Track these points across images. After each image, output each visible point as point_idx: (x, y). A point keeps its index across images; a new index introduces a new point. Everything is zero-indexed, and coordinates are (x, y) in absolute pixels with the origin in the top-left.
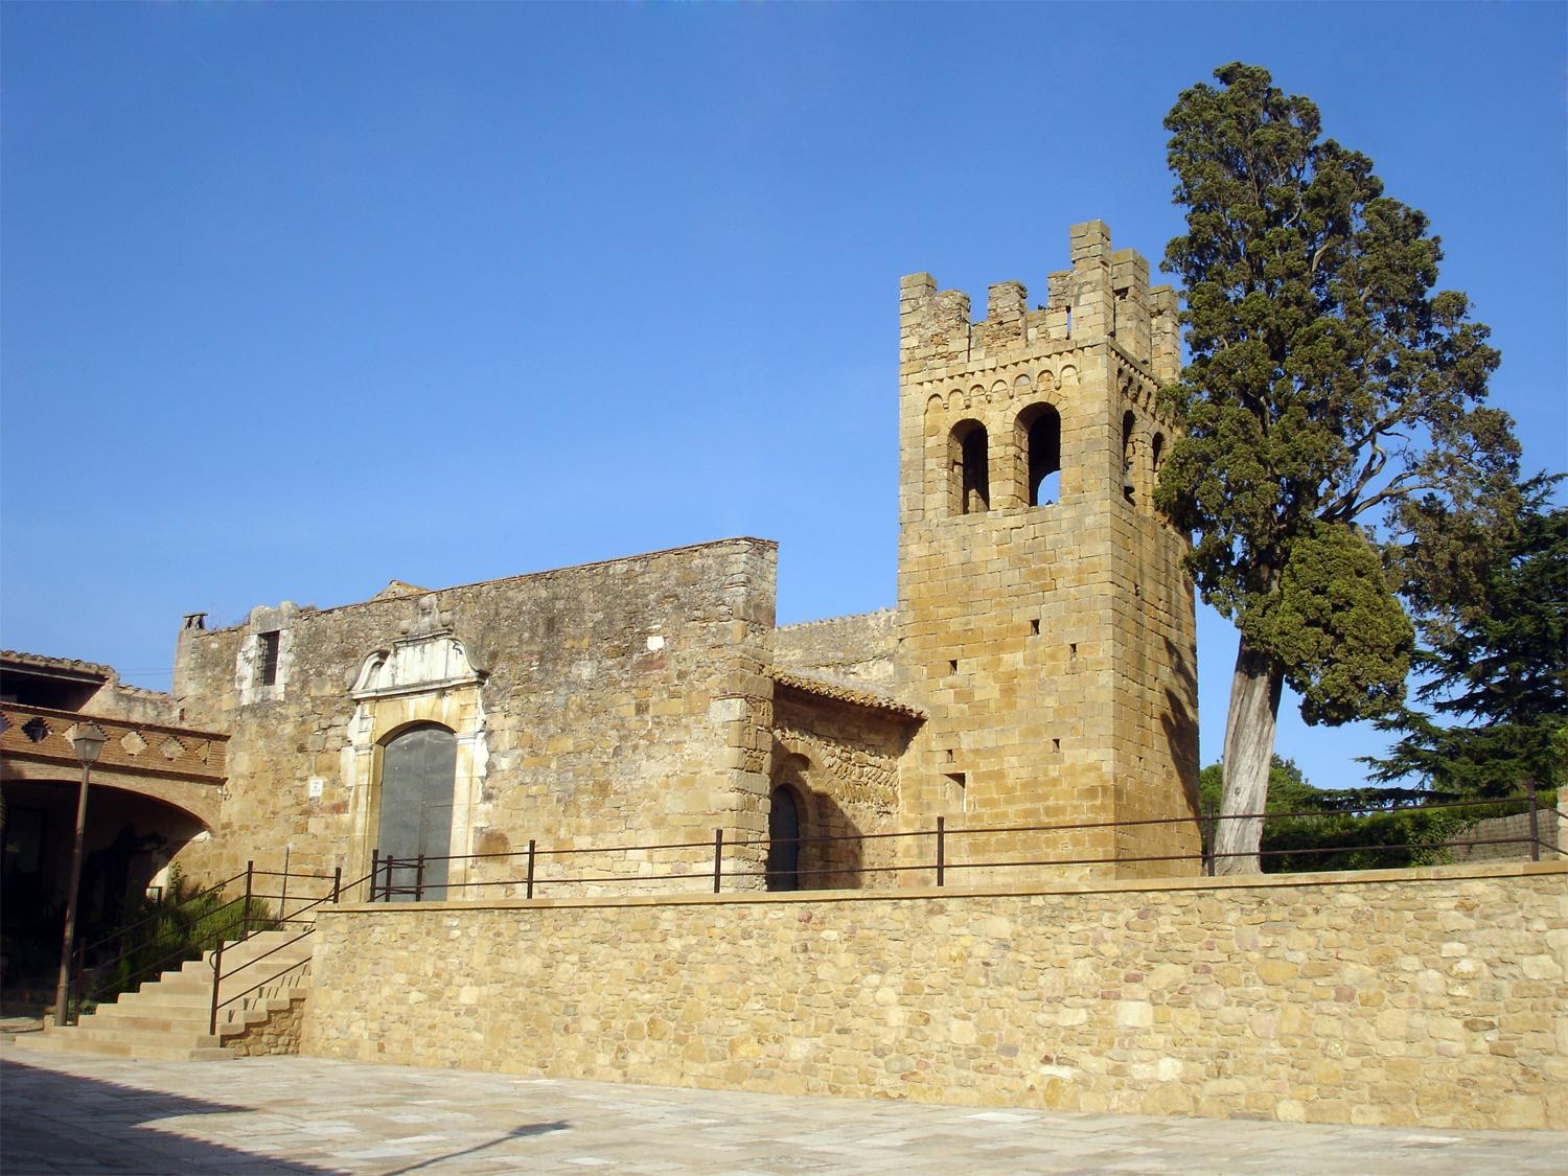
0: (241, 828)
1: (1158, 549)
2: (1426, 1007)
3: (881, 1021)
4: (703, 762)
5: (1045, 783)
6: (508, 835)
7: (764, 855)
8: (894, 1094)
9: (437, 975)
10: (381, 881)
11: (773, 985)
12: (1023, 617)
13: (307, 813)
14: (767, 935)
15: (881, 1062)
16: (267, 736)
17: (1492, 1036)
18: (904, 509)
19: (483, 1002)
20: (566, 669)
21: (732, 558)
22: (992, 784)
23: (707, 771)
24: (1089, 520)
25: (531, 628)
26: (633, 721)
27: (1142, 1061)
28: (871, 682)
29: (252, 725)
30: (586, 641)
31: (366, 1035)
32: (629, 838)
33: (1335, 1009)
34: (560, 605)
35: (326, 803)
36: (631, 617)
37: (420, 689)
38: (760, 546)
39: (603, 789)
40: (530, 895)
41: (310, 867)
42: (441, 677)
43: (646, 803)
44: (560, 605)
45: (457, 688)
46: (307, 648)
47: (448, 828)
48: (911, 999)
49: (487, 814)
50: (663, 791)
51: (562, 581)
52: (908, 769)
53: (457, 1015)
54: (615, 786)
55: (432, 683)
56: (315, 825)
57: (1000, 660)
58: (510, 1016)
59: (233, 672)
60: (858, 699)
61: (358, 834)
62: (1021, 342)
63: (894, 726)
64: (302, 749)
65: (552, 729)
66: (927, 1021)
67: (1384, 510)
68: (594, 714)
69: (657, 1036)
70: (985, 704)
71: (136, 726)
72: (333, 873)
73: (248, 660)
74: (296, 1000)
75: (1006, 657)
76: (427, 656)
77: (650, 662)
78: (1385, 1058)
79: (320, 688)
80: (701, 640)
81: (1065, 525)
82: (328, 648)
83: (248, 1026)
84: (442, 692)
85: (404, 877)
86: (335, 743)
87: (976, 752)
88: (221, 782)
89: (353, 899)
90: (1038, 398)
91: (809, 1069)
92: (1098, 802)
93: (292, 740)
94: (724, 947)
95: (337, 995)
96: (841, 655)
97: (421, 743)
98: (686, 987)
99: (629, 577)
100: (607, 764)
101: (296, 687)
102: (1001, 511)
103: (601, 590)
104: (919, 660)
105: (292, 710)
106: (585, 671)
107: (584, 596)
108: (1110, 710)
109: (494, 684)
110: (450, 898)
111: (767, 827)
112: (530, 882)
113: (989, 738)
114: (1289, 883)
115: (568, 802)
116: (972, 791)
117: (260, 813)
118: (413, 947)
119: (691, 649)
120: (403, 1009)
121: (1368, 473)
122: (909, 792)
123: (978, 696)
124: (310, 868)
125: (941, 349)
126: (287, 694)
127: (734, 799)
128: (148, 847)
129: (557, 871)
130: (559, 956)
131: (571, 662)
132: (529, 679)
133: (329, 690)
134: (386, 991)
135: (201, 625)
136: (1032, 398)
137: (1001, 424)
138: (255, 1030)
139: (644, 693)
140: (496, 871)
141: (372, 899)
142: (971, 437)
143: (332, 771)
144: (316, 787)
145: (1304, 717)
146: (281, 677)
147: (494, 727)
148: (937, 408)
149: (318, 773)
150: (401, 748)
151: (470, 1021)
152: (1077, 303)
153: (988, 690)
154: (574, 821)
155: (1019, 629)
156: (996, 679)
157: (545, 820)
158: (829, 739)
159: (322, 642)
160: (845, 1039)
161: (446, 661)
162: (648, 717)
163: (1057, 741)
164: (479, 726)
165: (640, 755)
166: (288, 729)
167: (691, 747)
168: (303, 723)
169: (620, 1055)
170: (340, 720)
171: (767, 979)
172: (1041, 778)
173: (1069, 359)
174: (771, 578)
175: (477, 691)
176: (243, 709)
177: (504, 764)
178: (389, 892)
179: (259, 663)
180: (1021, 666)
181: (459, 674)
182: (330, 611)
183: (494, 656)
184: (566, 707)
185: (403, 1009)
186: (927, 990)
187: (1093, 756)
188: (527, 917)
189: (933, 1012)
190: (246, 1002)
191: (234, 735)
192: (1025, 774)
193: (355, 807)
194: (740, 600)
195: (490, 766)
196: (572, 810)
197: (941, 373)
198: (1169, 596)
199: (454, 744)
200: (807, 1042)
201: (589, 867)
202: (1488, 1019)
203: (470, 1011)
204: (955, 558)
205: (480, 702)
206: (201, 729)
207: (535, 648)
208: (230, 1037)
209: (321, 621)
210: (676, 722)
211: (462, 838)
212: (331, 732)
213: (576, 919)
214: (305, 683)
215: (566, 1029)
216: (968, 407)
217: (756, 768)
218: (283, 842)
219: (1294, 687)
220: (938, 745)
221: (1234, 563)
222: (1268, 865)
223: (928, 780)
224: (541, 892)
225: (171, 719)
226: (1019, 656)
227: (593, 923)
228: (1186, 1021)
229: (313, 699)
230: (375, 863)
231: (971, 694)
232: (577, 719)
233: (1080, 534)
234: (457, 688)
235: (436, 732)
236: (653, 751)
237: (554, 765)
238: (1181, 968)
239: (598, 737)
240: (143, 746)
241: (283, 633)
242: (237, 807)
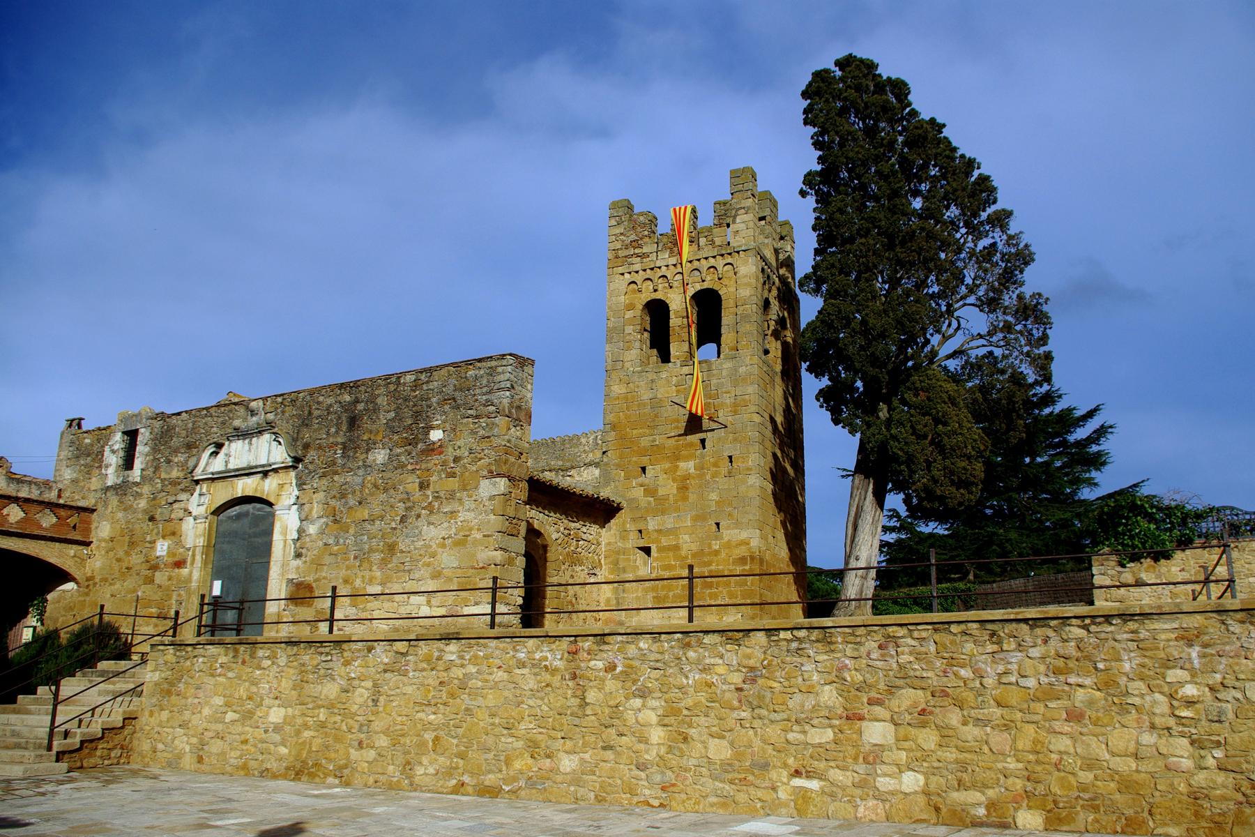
0: (101, 580)
2: (1153, 726)
3: (644, 740)
4: (468, 528)
5: (709, 554)
6: (314, 585)
7: (520, 601)
8: (656, 803)
9: (250, 698)
10: (206, 619)
11: (545, 708)
13: (155, 568)
14: (540, 667)
15: (643, 775)
16: (125, 510)
17: (1219, 753)
18: (609, 360)
19: (287, 720)
20: (364, 456)
21: (500, 369)
22: (671, 554)
24: (742, 370)
25: (337, 425)
27: (885, 775)
28: (583, 480)
29: (114, 500)
31: (187, 748)
32: (410, 586)
33: (1067, 729)
35: (170, 560)
36: (417, 415)
37: (247, 472)
38: (523, 362)
39: (392, 548)
40: (331, 631)
41: (154, 610)
42: (264, 462)
43: (426, 559)
44: (361, 406)
45: (276, 471)
46: (163, 438)
47: (265, 579)
48: (671, 720)
49: (298, 568)
51: (362, 388)
52: (609, 544)
53: (266, 732)
54: (402, 546)
55: (256, 467)
56: (160, 577)
57: (677, 467)
58: (312, 733)
59: (101, 461)
60: (578, 491)
61: (194, 585)
63: (600, 510)
64: (152, 519)
65: (352, 502)
66: (685, 739)
68: (386, 490)
69: (440, 751)
70: (665, 498)
71: (16, 500)
72: (172, 613)
73: (113, 452)
74: (129, 719)
75: (682, 465)
76: (254, 446)
78: (1117, 772)
80: (473, 433)
82: (175, 442)
83: (82, 742)
84: (265, 474)
85: (230, 617)
87: (659, 531)
88: (88, 544)
89: (188, 633)
90: (706, 285)
91: (576, 780)
93: (145, 511)
94: (501, 675)
95: (165, 715)
96: (560, 463)
97: (246, 514)
98: (467, 709)
99: (416, 385)
101: (150, 472)
102: (678, 363)
103: (394, 395)
104: (618, 466)
106: (380, 456)
107: (379, 400)
108: (757, 502)
109: (306, 468)
110: (266, 634)
111: (522, 579)
112: (332, 620)
113: (669, 522)
114: (1020, 617)
116: (656, 559)
117: (117, 568)
118: (230, 675)
119: (465, 441)
120: (220, 727)
122: (608, 560)
123: (661, 492)
124: (154, 611)
125: (637, 251)
126: (142, 477)
127: (499, 556)
129: (352, 612)
130: (356, 683)
131: (368, 450)
133: (175, 473)
134: (206, 711)
135: (79, 426)
136: (676, 312)
137: (678, 302)
138: (90, 745)
139: (426, 474)
140: (306, 613)
141: (199, 635)
142: (657, 311)
144: (162, 548)
146: (138, 464)
148: (634, 291)
149: (164, 537)
150: (230, 518)
151: (277, 738)
152: (734, 222)
153: (668, 488)
154: (367, 574)
156: (674, 480)
157: (343, 573)
158: (554, 516)
160: (609, 755)
161: (270, 451)
162: (429, 493)
163: (718, 524)
164: (293, 500)
165: (421, 522)
166: (143, 504)
167: (462, 516)
169: (408, 767)
170: (183, 496)
171: (539, 702)
172: (707, 550)
173: (729, 260)
174: (529, 387)
175: (293, 474)
176: (108, 488)
177: (312, 529)
178: (214, 628)
179: (121, 454)
180: (692, 471)
181: (279, 459)
182: (179, 414)
183: (306, 447)
184: (363, 485)
185: (220, 727)
186: (685, 712)
187: (744, 535)
188: (327, 650)
189: (692, 732)
190: (80, 721)
191: (100, 508)
192: (694, 547)
193: (192, 563)
194: (506, 402)
195: (301, 531)
196: (365, 565)
197: (637, 267)
199: (273, 515)
200: (576, 758)
201: (378, 608)
202: (1215, 738)
203: (277, 728)
204: (646, 395)
205: (294, 482)
206: (73, 504)
207: (339, 440)
208: (64, 753)
209: (174, 421)
210: (452, 496)
211: (277, 586)
212: (176, 506)
213: (370, 650)
214: (157, 468)
215: (360, 743)
216: (655, 291)
217: (515, 532)
218: (135, 591)
222: (877, 610)
223: (625, 551)
224: (339, 630)
225: (51, 496)
226: (691, 464)
227: (382, 655)
228: (928, 738)
229: (163, 480)
230: (202, 605)
231: (657, 490)
232: (372, 494)
233: (736, 380)
234: (276, 471)
235: (258, 506)
236: (433, 518)
238: (920, 692)
239: (388, 508)
240: (22, 515)
241: (142, 430)
242: (98, 564)
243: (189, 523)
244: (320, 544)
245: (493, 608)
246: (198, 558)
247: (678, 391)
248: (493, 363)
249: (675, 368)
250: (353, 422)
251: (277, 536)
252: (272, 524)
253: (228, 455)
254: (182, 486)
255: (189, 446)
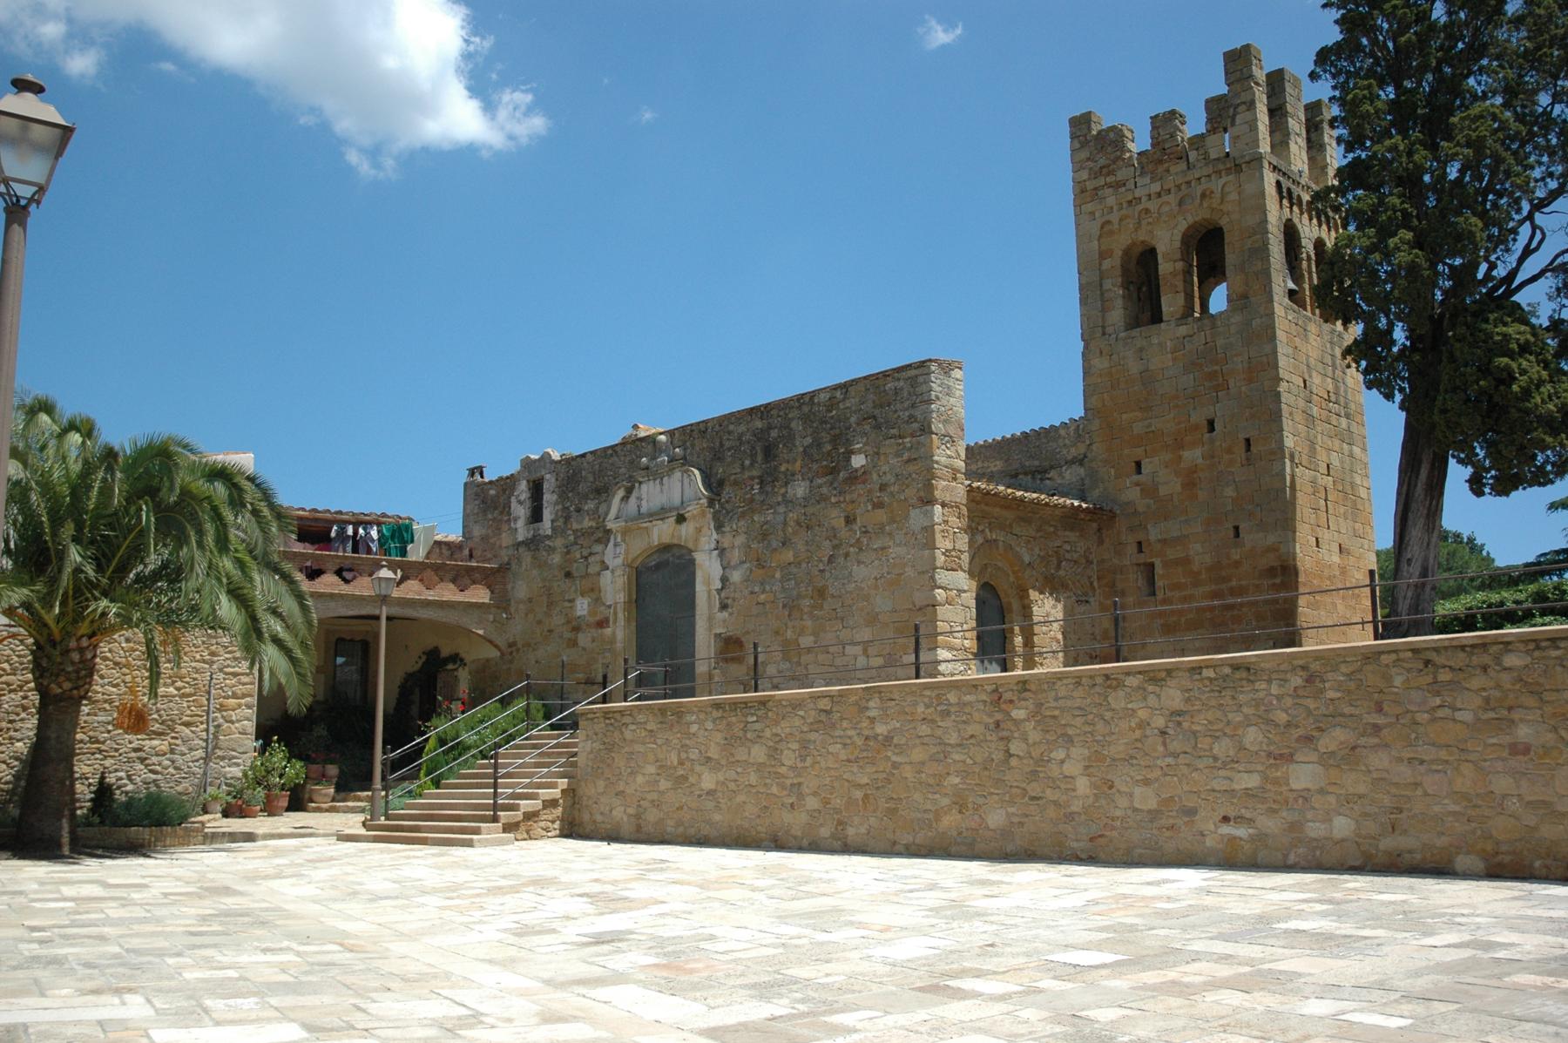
1: (1324, 345)
12: (1199, 417)
13: (577, 629)
23: (910, 572)
26: (844, 533)
29: (527, 557)
30: (798, 464)
34: (774, 433)
35: (592, 620)
36: (835, 440)
39: (821, 593)
44: (774, 433)
50: (873, 592)
51: (774, 412)
54: (831, 590)
56: (584, 639)
59: (509, 514)
61: (619, 646)
62: (1183, 166)
64: (568, 575)
65: (774, 544)
67: (1548, 283)
73: (520, 502)
75: (1186, 454)
77: (855, 477)
79: (580, 522)
81: (1233, 329)
82: (583, 488)
86: (593, 569)
87: (1164, 542)
92: (1278, 581)
94: (924, 729)
96: (1037, 463)
100: (822, 571)
101: (560, 523)
103: (806, 419)
105: (559, 543)
106: (800, 489)
115: (791, 607)
121: (1527, 252)
123: (1163, 491)
126: (553, 529)
128: (450, 667)
131: (786, 484)
132: (752, 500)
133: (587, 523)
134: (640, 779)
143: (594, 592)
144: (582, 607)
145: (1472, 489)
146: (547, 515)
147: (726, 545)
152: (1233, 124)
153: (1170, 485)
155: (1196, 427)
159: (578, 483)
162: (856, 527)
164: (713, 546)
166: (556, 559)
167: (894, 551)
168: (568, 553)
170: (598, 548)
176: (519, 544)
177: (736, 576)
179: (528, 504)
180: (1200, 461)
185: (655, 796)
192: (1208, 559)
195: (724, 580)
198: (1337, 388)
203: (710, 793)
204: (1134, 367)
207: (755, 473)
212: (591, 559)
214: (567, 519)
219: (1460, 461)
220: (1130, 540)
221: (1395, 349)
228: (1354, 782)
232: (795, 533)
236: (862, 557)
237: (778, 575)
243: (606, 578)
244: (746, 592)
245: (917, 657)
246: (620, 615)
247: (1174, 359)
248: (913, 372)
249: (1168, 332)
250: (769, 452)
251: (700, 587)
252: (694, 574)
253: (639, 499)
254: (596, 536)
255: (598, 492)
